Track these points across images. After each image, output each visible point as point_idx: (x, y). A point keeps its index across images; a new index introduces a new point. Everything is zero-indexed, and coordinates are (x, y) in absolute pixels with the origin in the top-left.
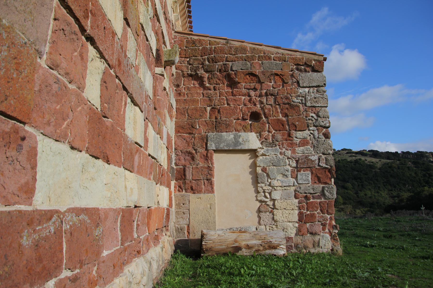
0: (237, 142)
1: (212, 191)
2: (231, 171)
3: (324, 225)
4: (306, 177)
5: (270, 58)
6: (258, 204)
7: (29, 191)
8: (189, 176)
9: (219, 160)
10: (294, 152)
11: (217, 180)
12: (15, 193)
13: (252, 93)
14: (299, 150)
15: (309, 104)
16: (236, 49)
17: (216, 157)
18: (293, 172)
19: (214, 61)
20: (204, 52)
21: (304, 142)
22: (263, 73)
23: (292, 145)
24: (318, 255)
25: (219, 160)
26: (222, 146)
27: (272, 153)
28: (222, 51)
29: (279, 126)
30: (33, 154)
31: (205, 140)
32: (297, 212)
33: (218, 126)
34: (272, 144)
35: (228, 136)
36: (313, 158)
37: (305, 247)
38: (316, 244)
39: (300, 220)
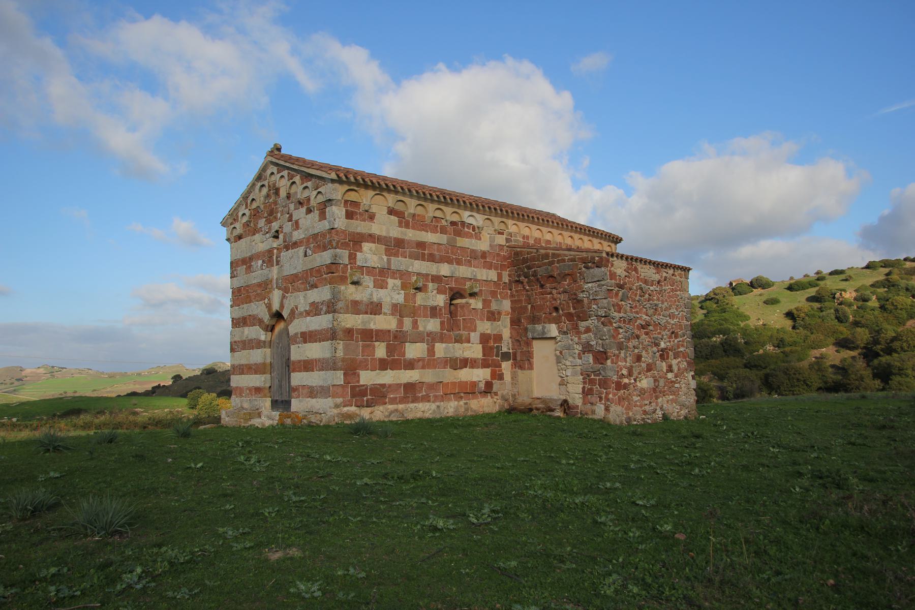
0: (544, 333)
1: (531, 368)
2: (542, 351)
3: (601, 398)
4: (590, 358)
5: (564, 261)
6: (560, 379)
7: (358, 381)
8: (518, 358)
9: (536, 344)
10: (579, 338)
11: (536, 361)
12: (821, 283)
13: (554, 291)
14: (583, 336)
15: (591, 298)
16: (543, 255)
17: (535, 343)
18: (579, 354)
19: (529, 268)
20: (525, 261)
21: (588, 330)
22: (559, 274)
23: (578, 333)
24: (594, 420)
25: (536, 344)
26: (536, 335)
27: (566, 340)
28: (533, 259)
29: (570, 316)
30: (359, 376)
31: (526, 330)
32: (581, 386)
33: (534, 320)
34: (565, 333)
35: (539, 327)
36: (592, 343)
37: (587, 414)
38: (593, 412)
39: (583, 392)
